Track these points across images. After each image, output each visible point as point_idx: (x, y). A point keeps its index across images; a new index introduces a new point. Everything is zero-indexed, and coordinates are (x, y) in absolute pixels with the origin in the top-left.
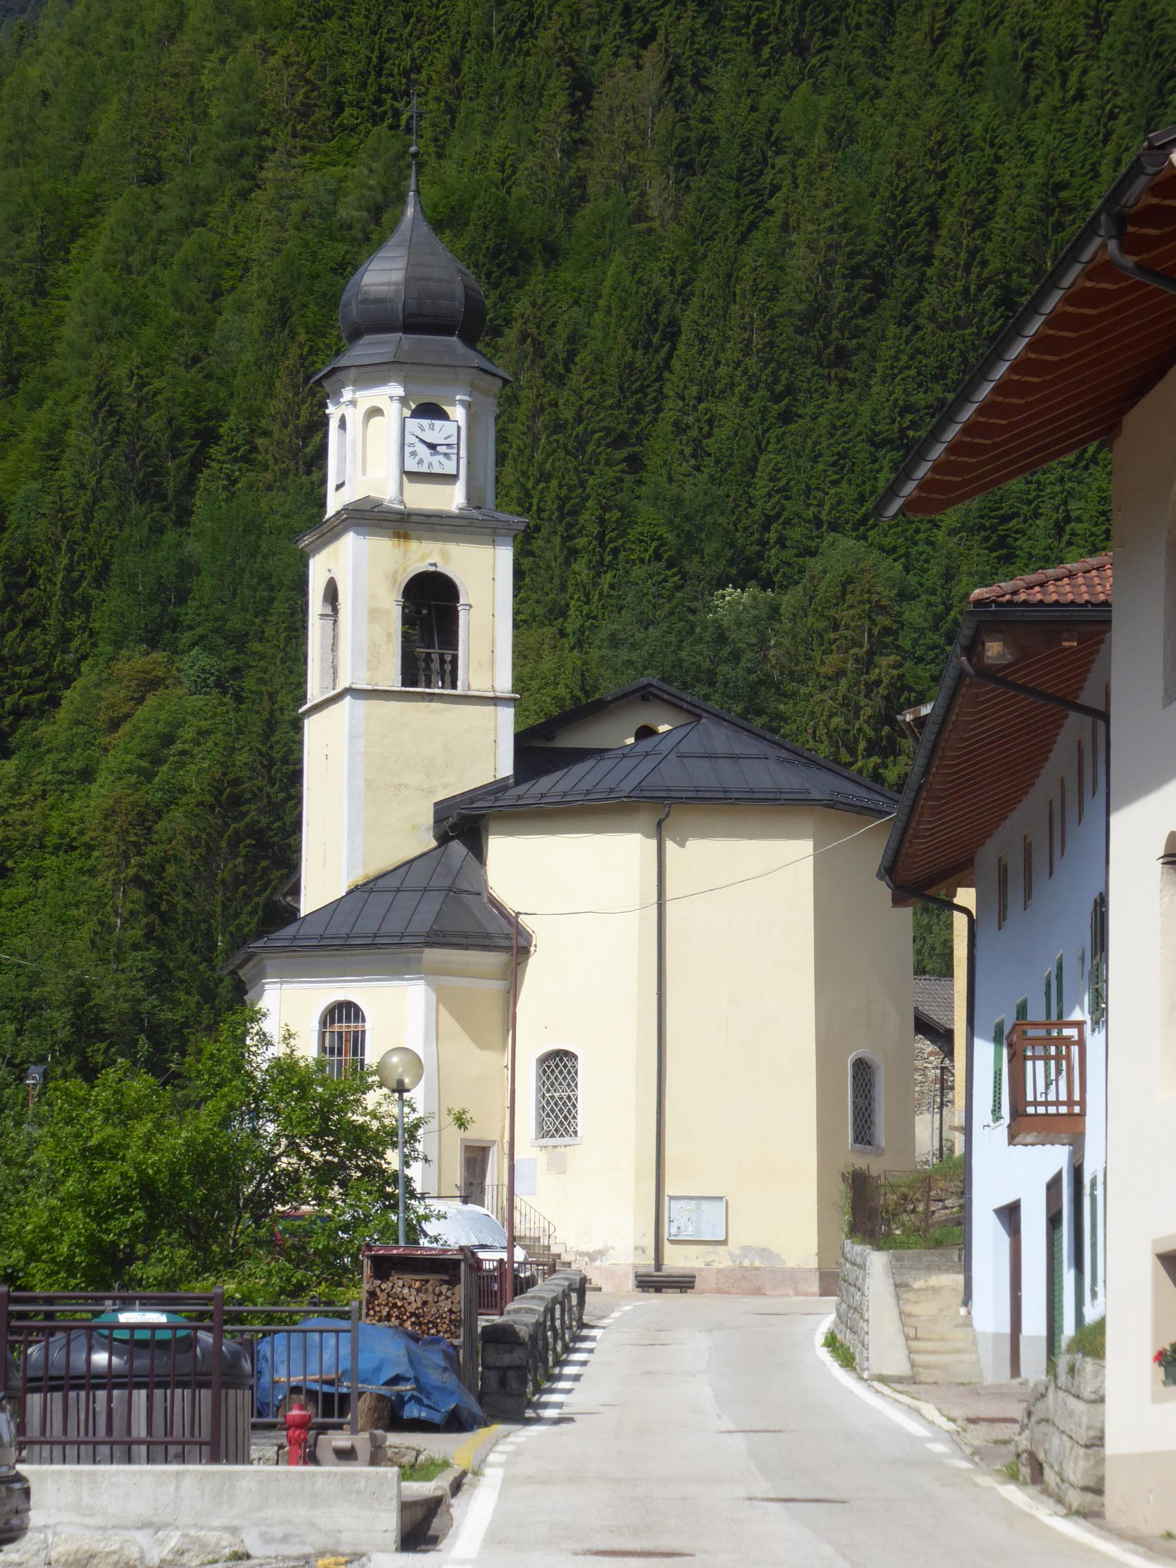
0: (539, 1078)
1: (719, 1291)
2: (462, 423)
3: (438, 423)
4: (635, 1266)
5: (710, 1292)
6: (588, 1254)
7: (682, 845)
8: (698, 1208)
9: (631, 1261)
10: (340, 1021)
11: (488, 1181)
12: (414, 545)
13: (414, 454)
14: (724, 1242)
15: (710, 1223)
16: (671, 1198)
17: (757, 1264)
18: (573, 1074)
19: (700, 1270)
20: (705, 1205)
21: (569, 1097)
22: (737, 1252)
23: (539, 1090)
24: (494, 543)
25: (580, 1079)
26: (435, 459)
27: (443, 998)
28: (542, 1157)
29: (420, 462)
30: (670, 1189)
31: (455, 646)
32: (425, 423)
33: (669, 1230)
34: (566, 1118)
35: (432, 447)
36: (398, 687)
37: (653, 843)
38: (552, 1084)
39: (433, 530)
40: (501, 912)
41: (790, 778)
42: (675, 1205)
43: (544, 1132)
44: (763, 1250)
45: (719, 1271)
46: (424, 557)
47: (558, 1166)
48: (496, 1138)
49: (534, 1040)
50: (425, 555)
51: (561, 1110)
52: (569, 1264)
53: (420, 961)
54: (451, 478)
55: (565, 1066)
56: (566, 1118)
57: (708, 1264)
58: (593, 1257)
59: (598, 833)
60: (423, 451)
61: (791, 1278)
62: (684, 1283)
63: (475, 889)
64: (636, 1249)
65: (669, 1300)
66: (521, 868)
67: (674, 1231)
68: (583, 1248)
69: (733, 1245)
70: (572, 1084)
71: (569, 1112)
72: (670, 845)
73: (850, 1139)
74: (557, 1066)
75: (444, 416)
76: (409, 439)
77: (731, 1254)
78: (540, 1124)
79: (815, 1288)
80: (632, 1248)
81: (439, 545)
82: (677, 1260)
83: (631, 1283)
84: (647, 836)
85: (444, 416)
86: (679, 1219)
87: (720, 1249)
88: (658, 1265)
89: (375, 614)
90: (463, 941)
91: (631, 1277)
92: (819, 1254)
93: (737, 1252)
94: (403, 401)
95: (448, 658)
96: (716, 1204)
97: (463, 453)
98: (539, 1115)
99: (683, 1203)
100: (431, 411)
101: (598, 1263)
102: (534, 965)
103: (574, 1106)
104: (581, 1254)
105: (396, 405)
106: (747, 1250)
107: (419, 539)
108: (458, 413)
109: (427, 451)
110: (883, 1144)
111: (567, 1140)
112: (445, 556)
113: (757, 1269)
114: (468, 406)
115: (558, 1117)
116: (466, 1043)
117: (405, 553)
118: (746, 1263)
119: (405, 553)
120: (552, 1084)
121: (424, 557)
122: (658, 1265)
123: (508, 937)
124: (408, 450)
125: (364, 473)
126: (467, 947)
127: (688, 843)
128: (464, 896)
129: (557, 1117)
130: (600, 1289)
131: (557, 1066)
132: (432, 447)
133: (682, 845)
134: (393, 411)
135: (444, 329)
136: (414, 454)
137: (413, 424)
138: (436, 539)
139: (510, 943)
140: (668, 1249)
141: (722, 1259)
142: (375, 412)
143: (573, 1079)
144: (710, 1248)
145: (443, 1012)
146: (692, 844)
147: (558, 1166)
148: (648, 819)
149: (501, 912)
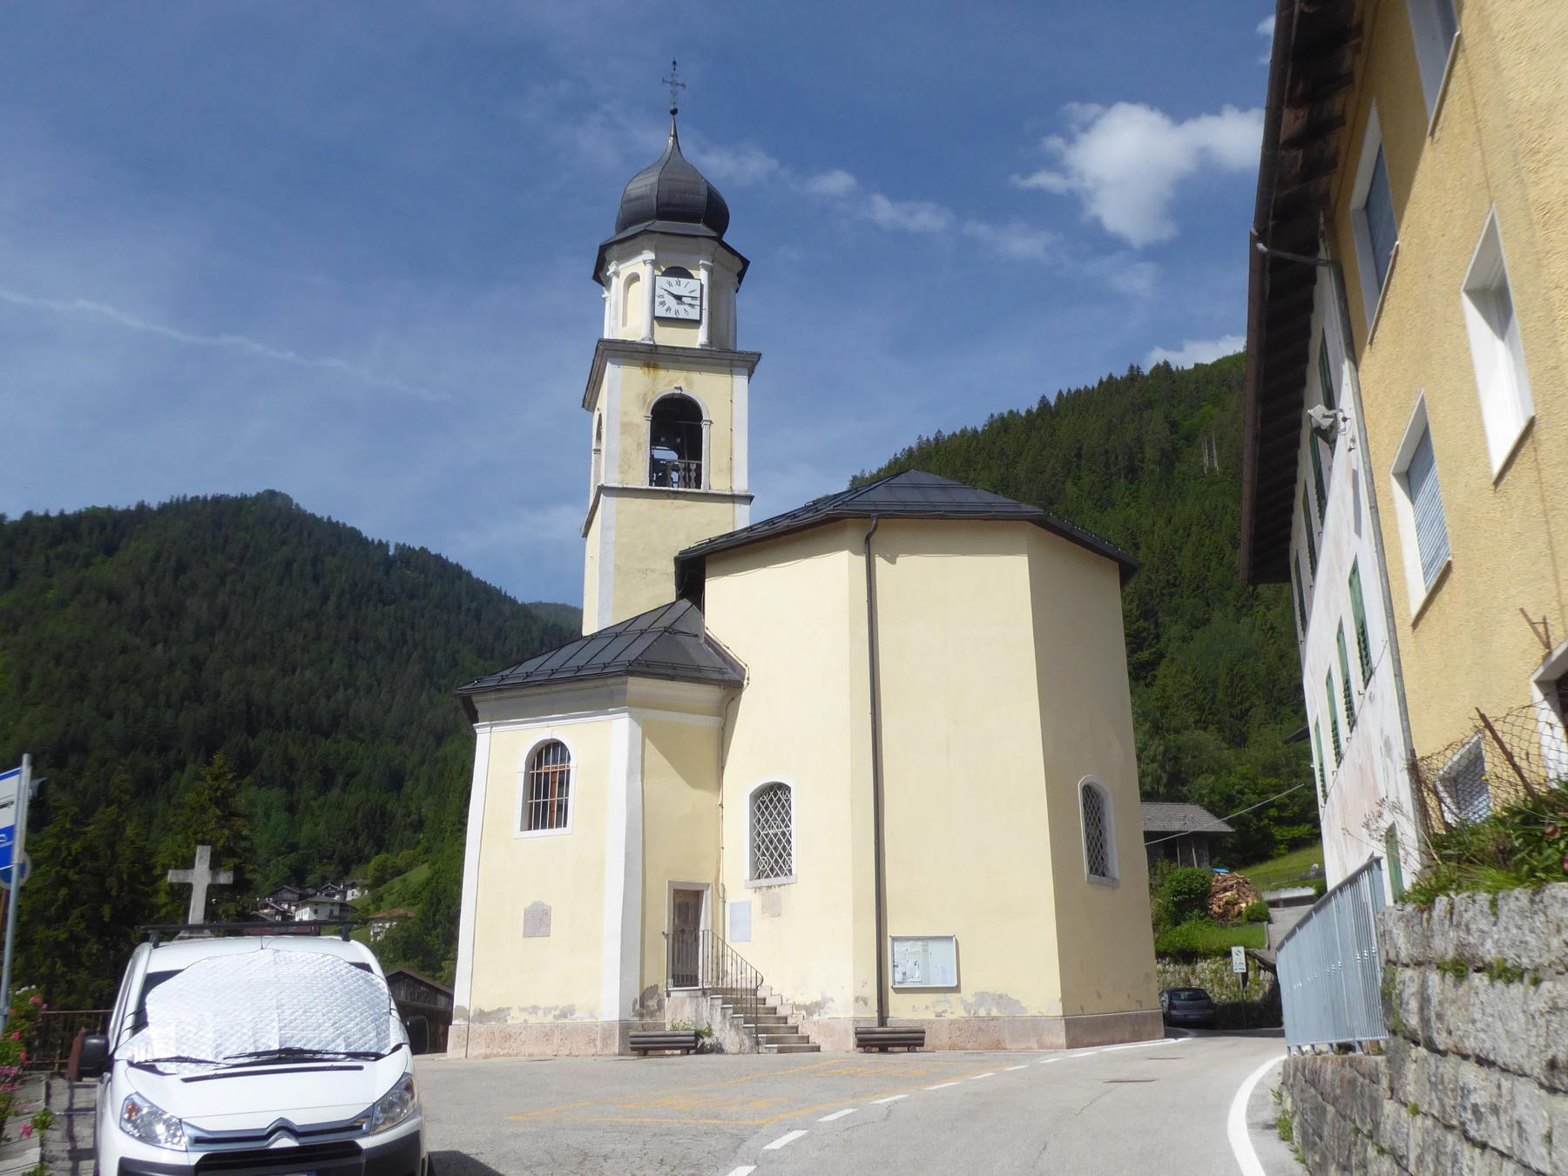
0: (753, 814)
1: (952, 1047)
2: (705, 281)
3: (684, 281)
4: (856, 1021)
5: (942, 1048)
6: (805, 1007)
7: (893, 562)
8: (925, 951)
9: (851, 1014)
10: (555, 762)
11: (702, 927)
12: (662, 373)
13: (663, 303)
14: (957, 989)
15: (940, 973)
16: (894, 939)
17: (995, 1013)
18: (786, 807)
19: (930, 1022)
20: (932, 946)
21: (784, 834)
22: (971, 1000)
23: (753, 828)
24: (731, 373)
25: (793, 813)
26: (681, 308)
27: (649, 733)
28: (756, 899)
29: (669, 309)
30: (893, 930)
31: (700, 459)
32: (673, 280)
33: (893, 977)
34: (781, 856)
35: (679, 298)
36: (647, 486)
37: (862, 560)
38: (767, 821)
39: (678, 361)
40: (716, 651)
41: (1001, 501)
42: (899, 947)
43: (758, 872)
44: (1001, 996)
45: (952, 1022)
46: (670, 383)
47: (773, 909)
48: (710, 880)
49: (744, 774)
50: (670, 382)
51: (776, 848)
52: (785, 1019)
53: (624, 692)
54: (696, 323)
55: (779, 800)
56: (781, 856)
57: (939, 1015)
58: (811, 1009)
59: (806, 557)
60: (671, 302)
61: (1033, 1027)
62: (912, 1040)
63: (693, 631)
64: (857, 999)
65: (899, 1060)
66: (735, 607)
67: (899, 977)
68: (799, 1000)
69: (967, 993)
70: (786, 820)
71: (784, 849)
72: (880, 563)
73: (1086, 870)
74: (771, 801)
75: (690, 276)
76: (659, 291)
77: (963, 1002)
78: (755, 864)
79: (1062, 1039)
80: (852, 999)
81: (684, 373)
82: (904, 1012)
83: (851, 1042)
84: (856, 553)
85: (690, 276)
86: (904, 961)
87: (952, 997)
88: (883, 1019)
89: (626, 428)
90: (670, 672)
91: (852, 1032)
92: (1063, 1000)
93: (971, 1000)
94: (655, 264)
95: (693, 467)
96: (943, 945)
97: (705, 305)
98: (753, 854)
99: (907, 945)
100: (680, 272)
101: (816, 1017)
102: (749, 698)
103: (789, 842)
104: (798, 1007)
105: (649, 267)
106: (982, 997)
107: (667, 369)
108: (702, 275)
109: (674, 301)
110: (1117, 876)
111: (782, 879)
112: (690, 383)
113: (994, 1019)
114: (711, 271)
115: (771, 856)
116: (676, 780)
117: (654, 380)
118: (982, 1013)
119: (654, 380)
120: (767, 821)
121: (670, 383)
122: (883, 1019)
123: (720, 671)
124: (657, 300)
125: (624, 324)
126: (672, 678)
127: (899, 560)
128: (679, 637)
129: (772, 855)
130: (818, 1049)
131: (771, 801)
132: (679, 298)
133: (893, 562)
134: (645, 272)
135: (693, 218)
136: (663, 303)
137: (663, 282)
138: (681, 369)
139: (726, 680)
140: (893, 999)
141: (955, 1009)
142: (634, 278)
143: (787, 813)
144: (941, 996)
145: (648, 741)
146: (902, 560)
147: (773, 909)
148: (854, 535)
149: (716, 651)
